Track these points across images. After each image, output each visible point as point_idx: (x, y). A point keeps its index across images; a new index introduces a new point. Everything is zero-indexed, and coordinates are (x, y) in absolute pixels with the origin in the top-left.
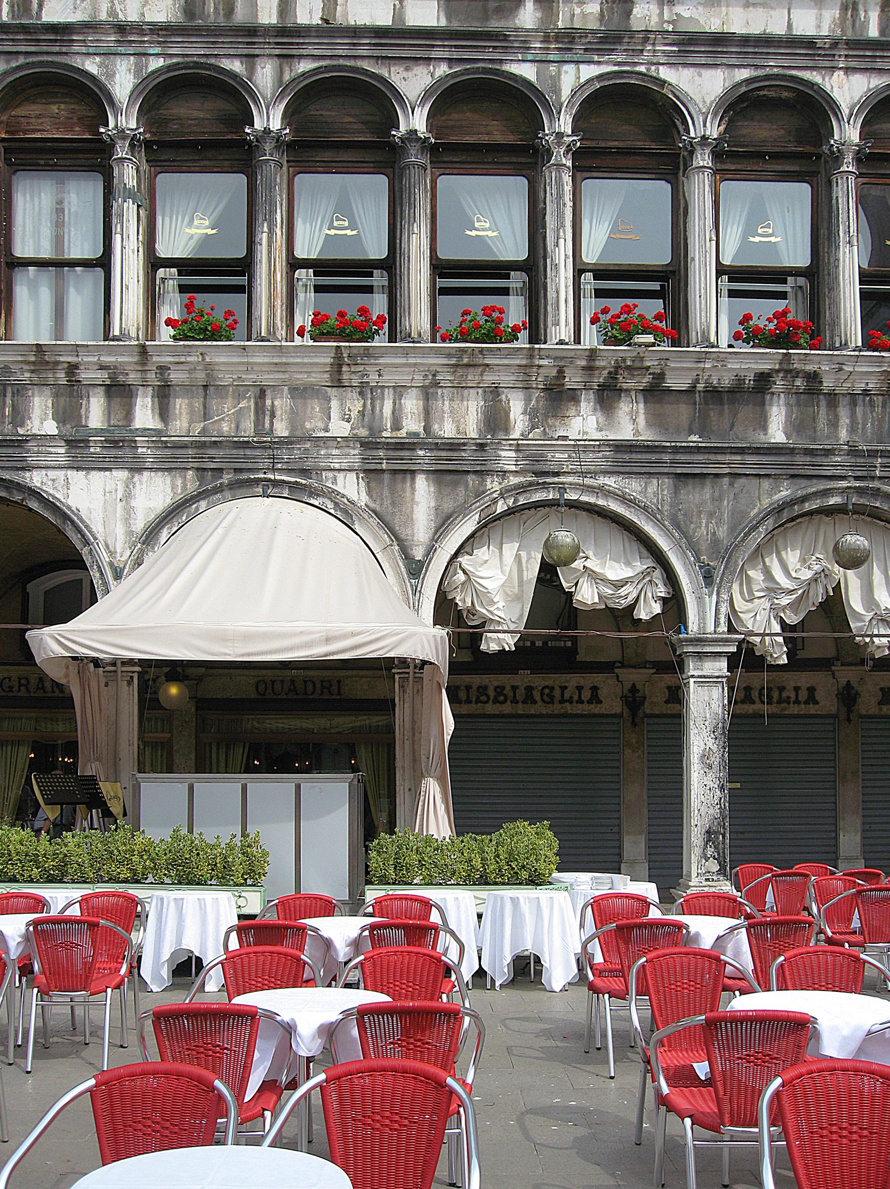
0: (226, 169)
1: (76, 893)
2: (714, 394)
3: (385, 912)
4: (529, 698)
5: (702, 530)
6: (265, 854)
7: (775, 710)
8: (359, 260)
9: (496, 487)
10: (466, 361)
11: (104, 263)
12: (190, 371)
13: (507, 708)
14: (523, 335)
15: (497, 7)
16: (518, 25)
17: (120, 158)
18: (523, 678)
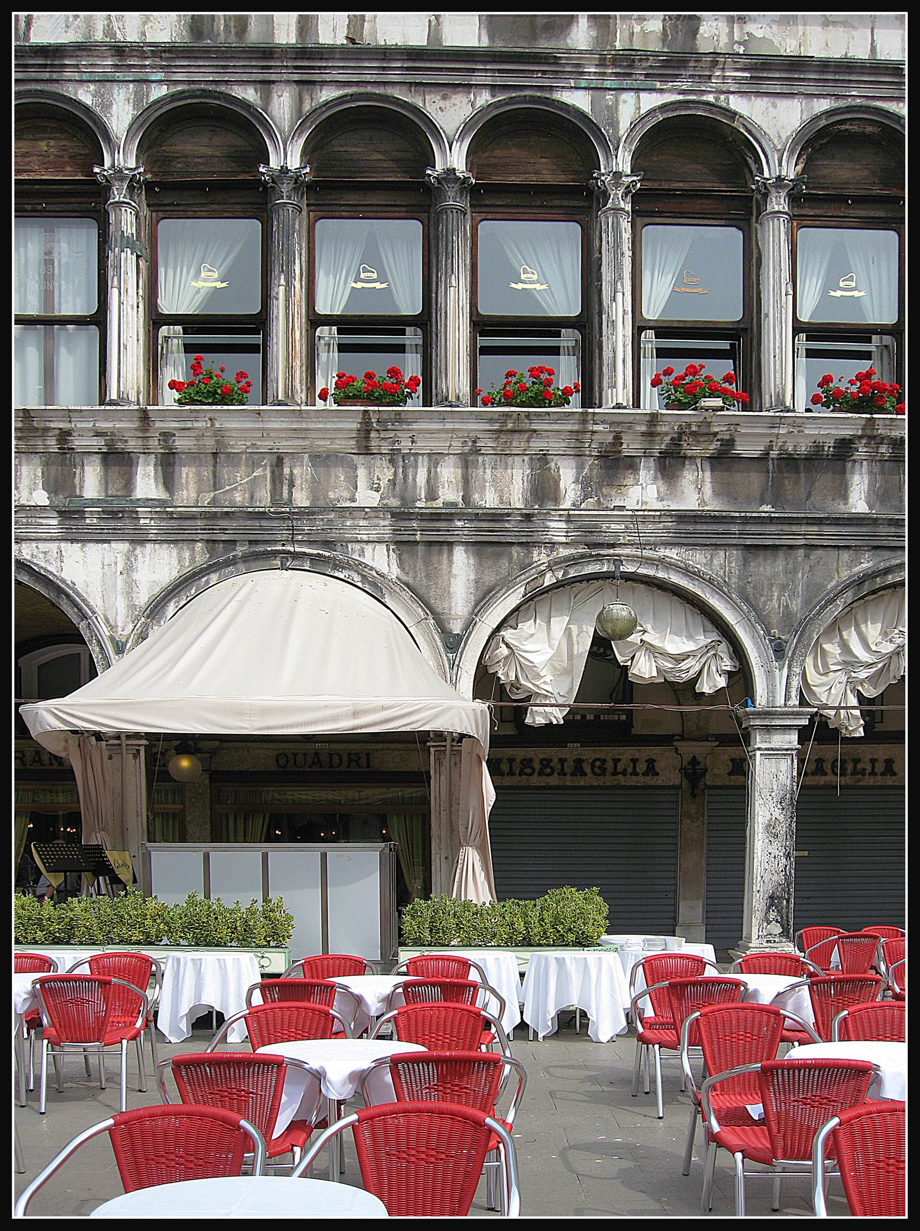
0: (237, 214)
1: (86, 953)
2: (789, 462)
3: (419, 970)
4: (578, 770)
5: (774, 604)
6: (289, 918)
7: (848, 782)
8: (389, 316)
9: (544, 558)
10: (510, 426)
11: (98, 320)
12: (197, 438)
13: (554, 780)
14: (575, 398)
15: (546, 24)
16: (571, 46)
17: (116, 202)
18: (573, 751)
